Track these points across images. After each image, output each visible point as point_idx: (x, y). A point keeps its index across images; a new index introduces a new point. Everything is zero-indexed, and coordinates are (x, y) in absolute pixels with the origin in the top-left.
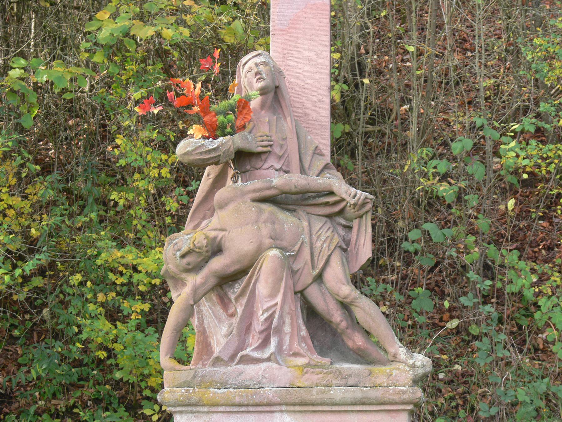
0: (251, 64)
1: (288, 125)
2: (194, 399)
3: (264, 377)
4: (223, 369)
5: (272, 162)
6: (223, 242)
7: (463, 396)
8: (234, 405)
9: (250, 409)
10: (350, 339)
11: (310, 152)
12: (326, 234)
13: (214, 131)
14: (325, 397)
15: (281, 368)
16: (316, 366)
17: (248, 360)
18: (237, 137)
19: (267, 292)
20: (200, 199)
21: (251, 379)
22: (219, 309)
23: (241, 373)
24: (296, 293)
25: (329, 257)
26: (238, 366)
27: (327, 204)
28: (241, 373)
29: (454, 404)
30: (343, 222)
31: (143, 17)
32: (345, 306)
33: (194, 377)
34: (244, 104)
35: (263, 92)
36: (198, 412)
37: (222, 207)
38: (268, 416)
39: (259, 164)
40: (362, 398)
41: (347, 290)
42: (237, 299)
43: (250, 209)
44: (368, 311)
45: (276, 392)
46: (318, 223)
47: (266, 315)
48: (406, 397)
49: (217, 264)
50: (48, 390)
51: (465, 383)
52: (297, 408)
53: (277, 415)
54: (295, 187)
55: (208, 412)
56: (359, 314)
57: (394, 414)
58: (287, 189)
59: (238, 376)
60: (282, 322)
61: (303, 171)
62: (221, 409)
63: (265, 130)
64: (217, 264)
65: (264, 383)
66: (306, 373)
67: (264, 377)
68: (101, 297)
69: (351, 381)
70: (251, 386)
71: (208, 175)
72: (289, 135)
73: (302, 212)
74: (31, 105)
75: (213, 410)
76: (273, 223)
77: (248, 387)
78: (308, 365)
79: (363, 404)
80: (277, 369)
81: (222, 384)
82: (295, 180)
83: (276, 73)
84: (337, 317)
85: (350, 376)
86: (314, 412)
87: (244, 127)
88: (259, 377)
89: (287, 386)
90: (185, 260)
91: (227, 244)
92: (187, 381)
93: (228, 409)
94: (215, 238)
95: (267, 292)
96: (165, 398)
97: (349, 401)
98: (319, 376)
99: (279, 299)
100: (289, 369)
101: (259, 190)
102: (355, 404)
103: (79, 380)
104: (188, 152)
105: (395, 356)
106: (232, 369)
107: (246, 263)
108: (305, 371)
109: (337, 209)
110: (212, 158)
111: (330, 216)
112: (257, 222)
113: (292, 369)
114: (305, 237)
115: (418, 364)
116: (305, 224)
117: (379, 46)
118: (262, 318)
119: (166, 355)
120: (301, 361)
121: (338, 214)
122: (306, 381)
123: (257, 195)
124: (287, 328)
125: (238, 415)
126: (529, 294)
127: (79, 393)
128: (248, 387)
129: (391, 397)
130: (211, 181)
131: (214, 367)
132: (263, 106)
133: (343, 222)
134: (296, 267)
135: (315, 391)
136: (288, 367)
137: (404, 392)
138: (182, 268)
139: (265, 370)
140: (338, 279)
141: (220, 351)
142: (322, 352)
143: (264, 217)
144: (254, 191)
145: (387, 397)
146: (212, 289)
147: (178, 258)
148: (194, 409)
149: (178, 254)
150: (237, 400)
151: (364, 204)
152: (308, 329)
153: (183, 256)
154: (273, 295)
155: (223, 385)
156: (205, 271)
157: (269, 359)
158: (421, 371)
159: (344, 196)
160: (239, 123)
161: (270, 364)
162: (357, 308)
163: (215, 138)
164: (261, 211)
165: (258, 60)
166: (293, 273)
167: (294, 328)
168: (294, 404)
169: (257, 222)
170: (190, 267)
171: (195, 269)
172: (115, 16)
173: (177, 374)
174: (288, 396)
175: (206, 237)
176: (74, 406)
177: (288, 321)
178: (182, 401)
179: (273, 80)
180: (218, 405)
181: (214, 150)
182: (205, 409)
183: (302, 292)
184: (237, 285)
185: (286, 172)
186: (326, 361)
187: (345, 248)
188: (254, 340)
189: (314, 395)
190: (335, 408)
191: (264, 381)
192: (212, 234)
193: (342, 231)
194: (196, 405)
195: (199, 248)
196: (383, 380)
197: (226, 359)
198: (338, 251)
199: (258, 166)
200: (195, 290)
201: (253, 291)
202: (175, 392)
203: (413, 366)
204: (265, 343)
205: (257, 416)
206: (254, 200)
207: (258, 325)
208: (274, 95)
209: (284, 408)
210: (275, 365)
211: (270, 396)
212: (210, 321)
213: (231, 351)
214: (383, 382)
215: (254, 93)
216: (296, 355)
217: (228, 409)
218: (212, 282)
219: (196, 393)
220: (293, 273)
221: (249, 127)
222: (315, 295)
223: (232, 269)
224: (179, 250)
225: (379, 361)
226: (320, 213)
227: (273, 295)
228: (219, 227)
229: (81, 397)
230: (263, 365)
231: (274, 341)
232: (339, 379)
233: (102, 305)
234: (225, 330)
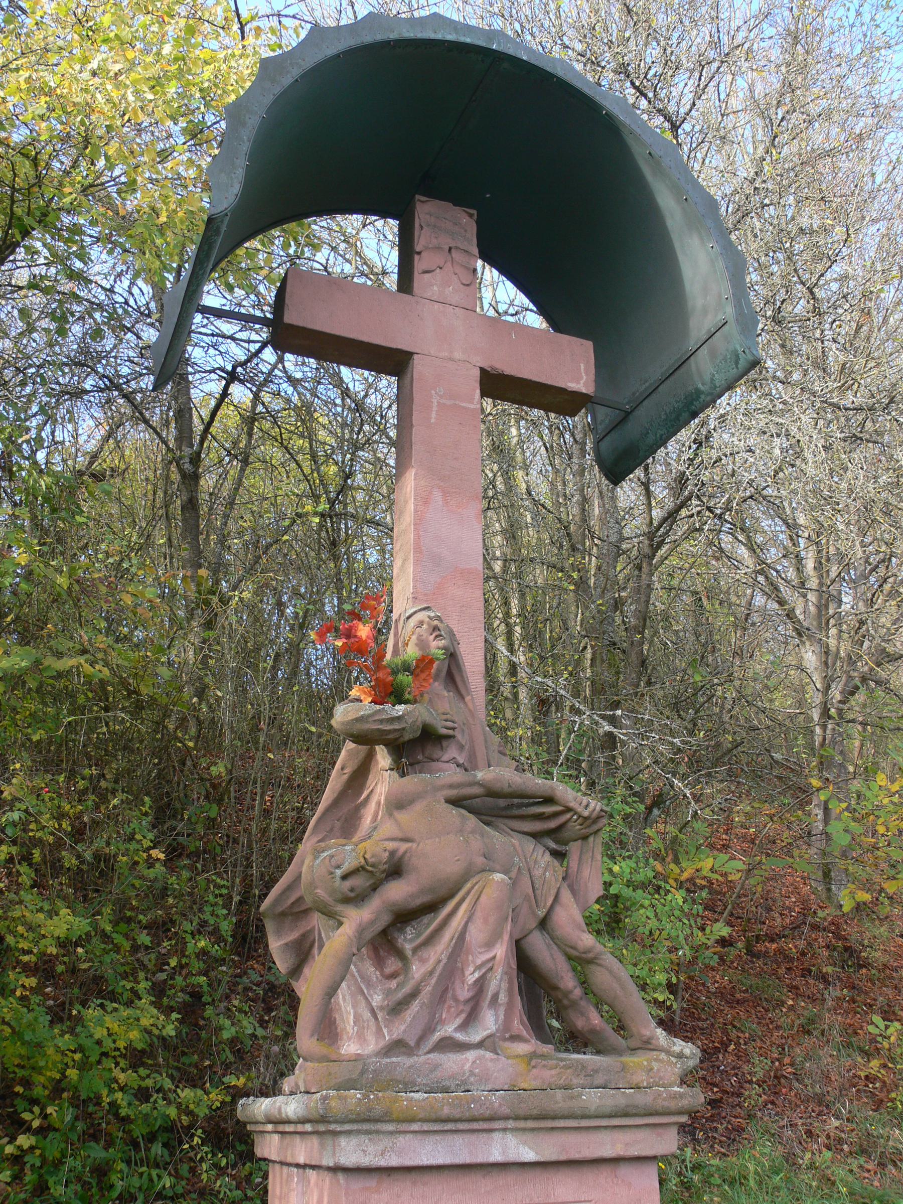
2: (378, 1110)
3: (472, 1073)
5: (452, 752)
6: (406, 858)
9: (460, 1126)
10: (582, 1014)
14: (574, 1105)
15: (498, 1060)
17: (448, 1045)
20: (330, 801)
21: (453, 1077)
26: (431, 1056)
27: (540, 817)
28: (436, 1067)
30: (553, 845)
32: (581, 962)
33: (362, 1073)
36: (377, 1132)
38: (483, 1137)
39: (437, 753)
40: (627, 1106)
45: (503, 1098)
47: (477, 975)
49: (398, 892)
52: (530, 1124)
53: (497, 1136)
54: (510, 786)
55: (392, 1133)
56: (600, 977)
57: (660, 1130)
58: (497, 787)
59: (431, 1071)
62: (415, 1127)
64: (398, 892)
65: (472, 1084)
66: (534, 1067)
67: (472, 1073)
69: (599, 1079)
70: (452, 1089)
71: (342, 769)
75: (402, 1129)
78: (533, 1055)
79: (626, 1115)
80: (492, 1060)
81: (406, 1084)
85: (596, 1071)
86: (553, 1129)
88: (464, 1074)
89: (506, 1087)
90: (348, 884)
92: (351, 1079)
93: (426, 1127)
94: (392, 853)
96: (330, 1108)
97: (607, 1110)
98: (553, 1072)
100: (510, 1061)
102: (610, 1116)
104: (362, 717)
105: (648, 1042)
108: (533, 1063)
109: (553, 824)
110: (395, 730)
112: (461, 831)
113: (514, 1061)
118: (471, 979)
119: (312, 1035)
122: (535, 1079)
123: (453, 793)
125: (438, 1137)
129: (666, 1104)
130: (346, 777)
131: (387, 1057)
133: (553, 845)
136: (508, 1058)
138: (339, 896)
139: (474, 1062)
141: (405, 1031)
144: (451, 786)
147: (338, 879)
148: (372, 1127)
149: (339, 872)
150: (446, 1111)
153: (344, 877)
157: (480, 1045)
159: (572, 804)
161: (481, 1052)
162: (599, 968)
168: (526, 1118)
170: (352, 895)
171: (357, 899)
174: (522, 1105)
178: (358, 1114)
180: (412, 1120)
181: (399, 718)
182: (390, 1127)
184: (408, 928)
189: (559, 1100)
190: (584, 1123)
191: (472, 1079)
194: (377, 1121)
195: (373, 866)
196: (641, 1078)
197: (412, 1043)
199: (435, 756)
202: (346, 1098)
205: (468, 1137)
209: (511, 1124)
210: (489, 1055)
211: (496, 1105)
214: (642, 1081)
217: (426, 1127)
223: (418, 902)
224: (338, 867)
225: (614, 1049)
226: (526, 830)
227: (489, 944)
228: (400, 835)
230: (471, 1055)
232: (582, 1076)
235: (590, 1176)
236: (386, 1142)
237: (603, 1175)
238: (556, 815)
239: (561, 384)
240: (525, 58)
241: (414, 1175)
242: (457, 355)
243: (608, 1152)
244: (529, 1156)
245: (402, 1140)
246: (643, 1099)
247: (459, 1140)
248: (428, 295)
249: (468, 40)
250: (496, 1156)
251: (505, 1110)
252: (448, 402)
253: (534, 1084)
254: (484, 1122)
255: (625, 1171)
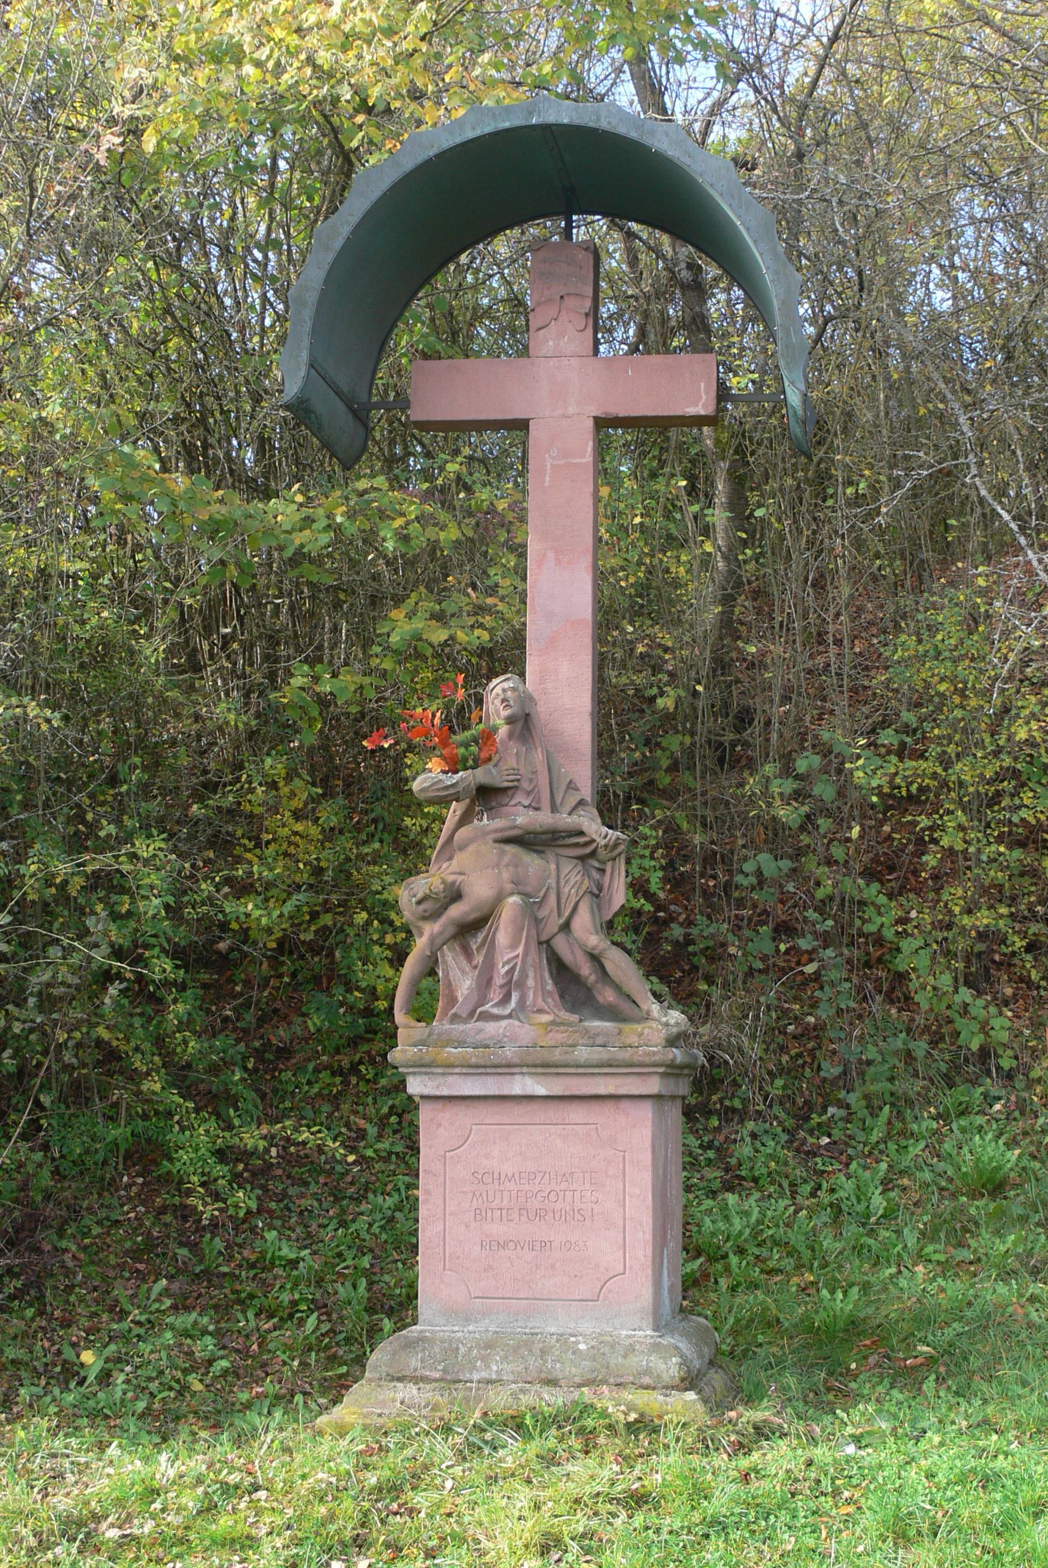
0: (498, 690)
1: (539, 756)
2: (427, 1059)
4: (461, 1027)
5: (520, 798)
7: (812, 1053)
8: (470, 1066)
11: (563, 787)
12: (575, 878)
13: (454, 766)
14: (568, 1058)
16: (562, 1024)
17: (486, 1017)
18: (479, 771)
19: (508, 944)
22: (462, 958)
23: (480, 1031)
24: (540, 943)
25: (577, 903)
28: (480, 1031)
29: (800, 1062)
30: (596, 864)
31: (440, 617)
32: (595, 958)
34: (489, 735)
35: (510, 720)
37: (462, 848)
39: (506, 800)
41: (595, 940)
42: (478, 949)
43: (489, 850)
44: (621, 965)
46: (567, 867)
48: (657, 1058)
49: (456, 911)
50: (330, 1045)
51: (817, 1037)
52: (540, 1070)
53: (518, 1078)
56: (609, 967)
58: (531, 828)
60: (524, 975)
61: (554, 809)
63: (512, 762)
68: (389, 939)
69: (599, 1041)
72: (540, 768)
73: (550, 855)
74: (311, 720)
76: (516, 866)
77: (487, 1047)
78: (553, 1023)
82: (544, 819)
83: (526, 700)
84: (586, 970)
87: (490, 759)
90: (421, 907)
91: (466, 890)
95: (508, 944)
99: (520, 950)
101: (502, 830)
103: (367, 1032)
106: (471, 1026)
107: (486, 910)
109: (588, 850)
111: (582, 858)
112: (498, 865)
114: (552, 881)
115: (672, 1022)
116: (553, 867)
117: (860, 610)
118: (503, 971)
120: (545, 1018)
121: (589, 856)
123: (499, 835)
124: (531, 982)
126: (889, 934)
127: (365, 1048)
128: (487, 1047)
132: (511, 735)
134: (541, 914)
135: (557, 1051)
137: (654, 1053)
140: (586, 929)
142: (573, 1009)
143: (506, 860)
145: (636, 1059)
146: (454, 937)
150: (473, 1060)
151: (616, 845)
152: (556, 984)
153: (419, 903)
154: (513, 946)
155: (461, 1043)
156: (443, 920)
158: (675, 1030)
160: (484, 755)
163: (456, 772)
164: (502, 853)
165: (506, 685)
166: (537, 921)
167: (538, 983)
168: (536, 1066)
169: (498, 865)
171: (433, 916)
172: (409, 616)
173: (412, 1032)
175: (444, 882)
176: (361, 1062)
177: (531, 974)
179: (523, 708)
180: (453, 1066)
181: (453, 785)
183: (548, 942)
185: (537, 809)
186: (574, 1018)
187: (597, 894)
188: (496, 995)
189: (557, 1055)
192: (451, 878)
193: (596, 875)
196: (634, 1040)
198: (587, 897)
200: (432, 939)
201: (493, 941)
203: (667, 1024)
204: (506, 999)
206: (496, 841)
207: (498, 980)
208: (523, 723)
212: (455, 973)
213: (470, 1007)
215: (500, 722)
216: (540, 1011)
218: (451, 930)
219: (428, 1053)
220: (537, 921)
221: (495, 759)
222: (560, 944)
227: (513, 946)
229: (368, 1053)
230: (504, 1023)
231: (515, 997)
233: (389, 947)
234: (468, 982)
235: (596, 1107)
236: (440, 1080)
237: (608, 1108)
238: (586, 844)
239: (679, 412)
240: (566, 121)
241: (468, 1102)
242: (571, 410)
243: (602, 1091)
244: (541, 1091)
245: (451, 1079)
246: (626, 1055)
247: (490, 1080)
248: (543, 352)
249: (507, 125)
250: (517, 1091)
251: (517, 1061)
252: (562, 462)
253: (551, 1043)
254: (506, 1068)
255: (625, 1104)
